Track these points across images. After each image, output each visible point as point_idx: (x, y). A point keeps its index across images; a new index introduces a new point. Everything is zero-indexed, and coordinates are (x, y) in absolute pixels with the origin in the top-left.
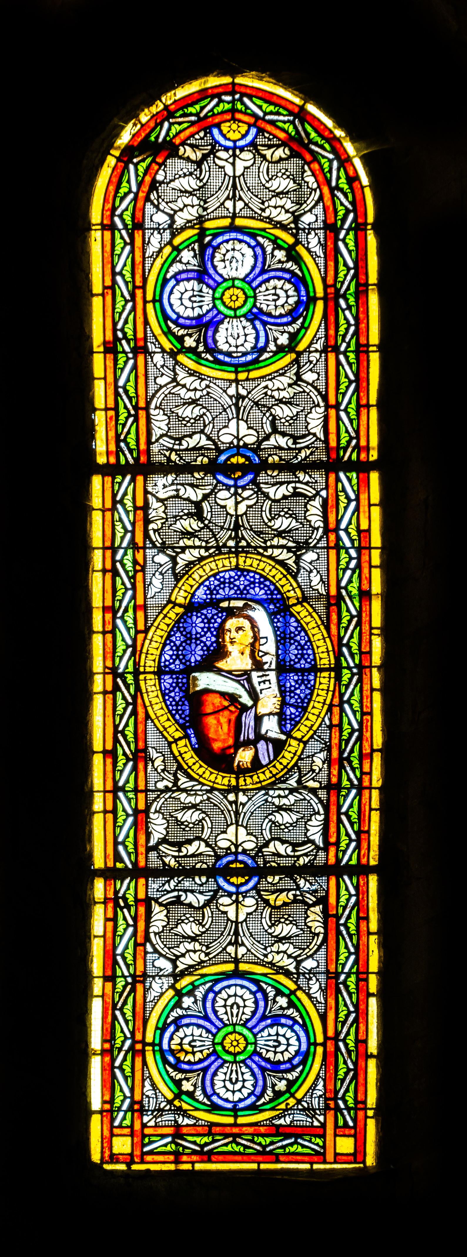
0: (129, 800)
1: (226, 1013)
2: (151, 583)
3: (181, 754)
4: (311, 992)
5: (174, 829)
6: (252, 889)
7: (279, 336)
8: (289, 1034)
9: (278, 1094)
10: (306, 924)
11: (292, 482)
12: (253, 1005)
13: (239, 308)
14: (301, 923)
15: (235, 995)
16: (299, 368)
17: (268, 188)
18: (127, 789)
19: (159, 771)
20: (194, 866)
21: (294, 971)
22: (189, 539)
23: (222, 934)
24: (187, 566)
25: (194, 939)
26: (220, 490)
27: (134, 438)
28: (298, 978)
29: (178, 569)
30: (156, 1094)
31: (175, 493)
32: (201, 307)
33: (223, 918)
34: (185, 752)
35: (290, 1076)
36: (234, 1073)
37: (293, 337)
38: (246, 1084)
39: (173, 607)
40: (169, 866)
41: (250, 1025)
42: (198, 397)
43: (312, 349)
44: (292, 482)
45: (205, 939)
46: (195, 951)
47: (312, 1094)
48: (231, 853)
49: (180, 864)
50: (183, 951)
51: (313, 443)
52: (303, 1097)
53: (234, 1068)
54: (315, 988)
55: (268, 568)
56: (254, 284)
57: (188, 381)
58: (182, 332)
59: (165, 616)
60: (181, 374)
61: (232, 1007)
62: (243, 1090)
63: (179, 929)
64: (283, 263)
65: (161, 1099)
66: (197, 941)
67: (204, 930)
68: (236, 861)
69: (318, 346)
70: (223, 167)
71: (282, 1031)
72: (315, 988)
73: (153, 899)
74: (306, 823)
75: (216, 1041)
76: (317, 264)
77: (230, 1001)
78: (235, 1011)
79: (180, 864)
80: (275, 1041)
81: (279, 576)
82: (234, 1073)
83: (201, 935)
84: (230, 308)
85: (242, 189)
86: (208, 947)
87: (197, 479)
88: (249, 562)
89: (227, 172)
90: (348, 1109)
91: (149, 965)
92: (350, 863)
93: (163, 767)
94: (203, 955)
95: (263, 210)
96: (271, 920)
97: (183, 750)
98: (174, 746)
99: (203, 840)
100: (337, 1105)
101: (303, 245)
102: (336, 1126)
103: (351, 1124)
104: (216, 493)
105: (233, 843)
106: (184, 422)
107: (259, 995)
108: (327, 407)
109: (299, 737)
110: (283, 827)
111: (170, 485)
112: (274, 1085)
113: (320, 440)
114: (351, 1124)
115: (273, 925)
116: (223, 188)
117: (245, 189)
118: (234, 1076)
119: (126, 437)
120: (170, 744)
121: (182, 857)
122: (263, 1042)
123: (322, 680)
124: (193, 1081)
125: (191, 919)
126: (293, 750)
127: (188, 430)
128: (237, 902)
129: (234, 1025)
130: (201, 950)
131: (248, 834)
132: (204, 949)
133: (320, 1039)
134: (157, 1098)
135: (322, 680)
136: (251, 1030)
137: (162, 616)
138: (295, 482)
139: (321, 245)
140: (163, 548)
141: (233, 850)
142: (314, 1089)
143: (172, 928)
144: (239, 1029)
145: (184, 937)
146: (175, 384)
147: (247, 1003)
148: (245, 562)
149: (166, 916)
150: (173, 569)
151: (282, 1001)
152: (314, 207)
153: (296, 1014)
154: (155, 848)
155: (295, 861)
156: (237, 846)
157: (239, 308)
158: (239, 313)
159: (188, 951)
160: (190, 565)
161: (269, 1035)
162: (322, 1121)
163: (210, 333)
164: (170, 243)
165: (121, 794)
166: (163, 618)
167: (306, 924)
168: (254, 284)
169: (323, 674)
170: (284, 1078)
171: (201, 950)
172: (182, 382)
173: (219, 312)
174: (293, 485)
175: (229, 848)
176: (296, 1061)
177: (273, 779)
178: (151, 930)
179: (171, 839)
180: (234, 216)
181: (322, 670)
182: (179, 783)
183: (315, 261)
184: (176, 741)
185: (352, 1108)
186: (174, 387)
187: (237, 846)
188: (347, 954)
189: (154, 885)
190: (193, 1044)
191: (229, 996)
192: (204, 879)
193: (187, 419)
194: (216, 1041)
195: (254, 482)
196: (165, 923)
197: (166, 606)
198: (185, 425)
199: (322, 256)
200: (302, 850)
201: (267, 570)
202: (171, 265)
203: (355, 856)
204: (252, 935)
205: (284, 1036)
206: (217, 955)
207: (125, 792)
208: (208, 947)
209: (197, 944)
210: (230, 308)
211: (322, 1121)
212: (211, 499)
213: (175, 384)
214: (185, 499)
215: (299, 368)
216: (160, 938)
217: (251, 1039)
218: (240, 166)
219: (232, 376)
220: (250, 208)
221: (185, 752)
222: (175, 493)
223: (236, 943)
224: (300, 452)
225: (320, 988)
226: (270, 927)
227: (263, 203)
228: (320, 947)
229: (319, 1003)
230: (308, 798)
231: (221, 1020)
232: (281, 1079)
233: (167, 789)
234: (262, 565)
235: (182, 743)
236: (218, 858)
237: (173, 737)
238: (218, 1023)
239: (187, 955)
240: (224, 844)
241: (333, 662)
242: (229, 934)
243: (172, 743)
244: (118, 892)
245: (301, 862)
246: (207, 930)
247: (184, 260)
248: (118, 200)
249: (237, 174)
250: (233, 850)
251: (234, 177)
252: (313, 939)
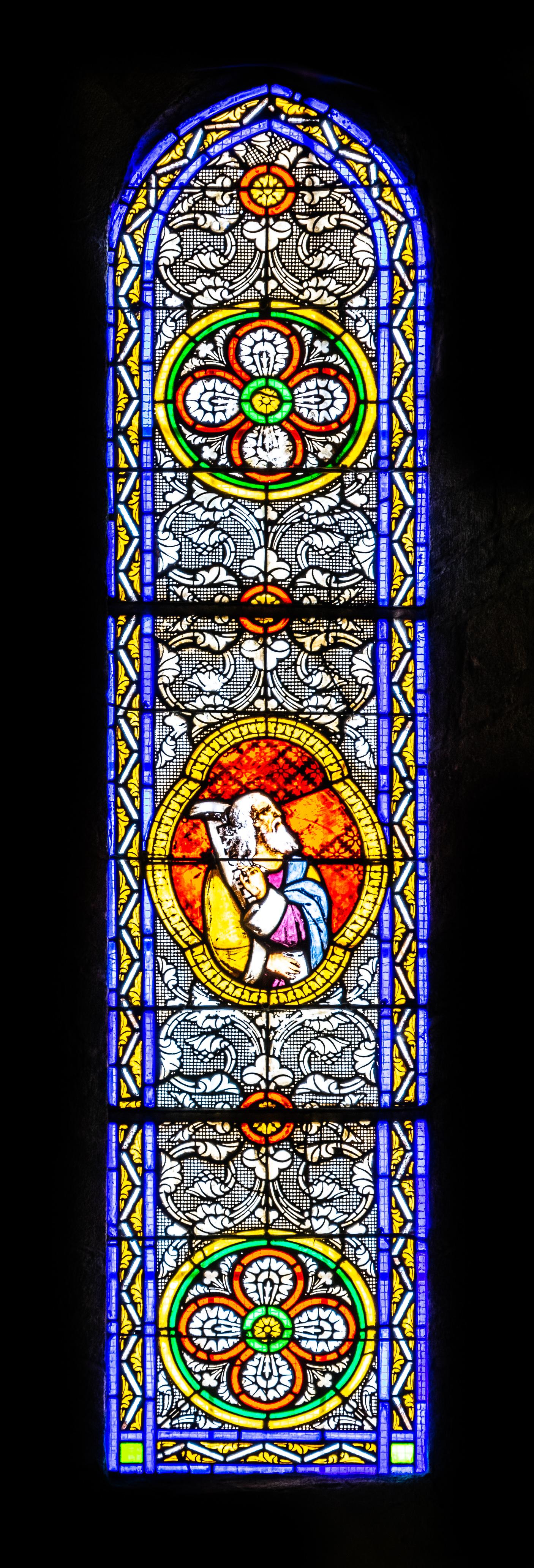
0: (132, 869)
1: (257, 1291)
2: (161, 749)
3: (197, 964)
4: (359, 1263)
5: (188, 1061)
6: (286, 211)
7: (321, 448)
8: (334, 1317)
9: (321, 1392)
10: (350, 674)
11: (336, 212)
12: (287, 351)
13: (272, 413)
14: (345, 673)
15: (269, 1270)
16: (343, 487)
17: (308, 685)
18: (129, 855)
19: (171, 987)
20: (213, 599)
21: (337, 730)
22: (209, 278)
23: (249, 267)
24: (205, 729)
25: (214, 1201)
26: (248, 221)
27: (140, 1217)
28: (342, 740)
29: (195, 732)
30: (172, 1390)
31: (192, 1150)
32: (224, 412)
33: (250, 248)
34: (203, 962)
35: (335, 1369)
36: (268, 1293)
37: (338, 449)
38: (282, 1380)
39: (187, 782)
40: (182, 1104)
41: (286, 1307)
42: (219, 1026)
43: (360, 466)
44: (336, 212)
45: (228, 272)
46: (215, 288)
47: (362, 1391)
48: (261, 1091)
49: (195, 596)
50: (202, 1216)
51: (360, 582)
52: (351, 1395)
53: (267, 1360)
54: (364, 1258)
55: (304, 737)
56: (293, 1313)
57: (206, 498)
58: (199, 440)
59: (177, 793)
60: (198, 490)
61: (264, 1284)
62: (279, 1387)
63: (196, 260)
64: (325, 355)
65: (178, 1395)
66: (218, 275)
67: (227, 1189)
68: (266, 1099)
69: (368, 461)
70: (253, 1169)
71: (209, 418)
72: (364, 1258)
73: (163, 1151)
74: (353, 1052)
75: (243, 397)
76: (368, 1285)
77: (263, 1277)
78: (264, 360)
79: (195, 596)
80: (216, 405)
81: (319, 746)
82: (268, 1293)
83: (222, 268)
84: (260, 413)
85: (275, 266)
86: (231, 283)
87: (219, 625)
88: (281, 729)
89: (258, 1174)
90: (407, 1339)
91: (159, 497)
92: (408, 1099)
93: (175, 983)
94: (225, 293)
95: (301, 292)
96: (308, 249)
97: (200, 959)
98: (188, 953)
99: (226, 1074)
100: (392, 1334)
101: (351, 1262)
102: (391, 1430)
103: (410, 1427)
104: (243, 224)
105: (262, 1078)
106: (201, 1057)
107: (293, 340)
108: (378, 538)
109: (344, 944)
110: (322, 552)
111: (347, 1094)
112: (316, 1381)
113: (369, 579)
114: (410, 1427)
115: (311, 255)
116: (253, 684)
117: (279, 265)
118: (267, 1370)
119: (129, 1357)
120: (183, 951)
121: (197, 587)
122: (302, 1330)
123: (373, 875)
124: (216, 1374)
125: (211, 1177)
126: (199, 767)
127: (205, 561)
128: (266, 574)
129: (267, 1306)
130: (223, 287)
131: (282, 1067)
132: (227, 284)
133: (372, 1321)
134: (173, 1396)
135: (373, 875)
136: (287, 1312)
137: (172, 793)
138: (340, 213)
139: (373, 1261)
140: (176, 710)
141: (262, 579)
142: (365, 1385)
143: (187, 260)
144: (273, 1311)
145: (333, 1036)
146: (189, 501)
147: (283, 1280)
148: (276, 729)
149: (180, 1172)
150: (189, 733)
151: (326, 1278)
152: (365, 1216)
153: (340, 361)
154: (165, 574)
155: (341, 1101)
156: (268, 1083)
157: (272, 413)
158: (271, 420)
159: (207, 1216)
160: (209, 728)
161: (308, 390)
162: (375, 1424)
163: (235, 446)
164: (184, 332)
165: (123, 862)
166: (175, 796)
167: (350, 674)
168: (293, 1313)
169: (374, 868)
170: (328, 1372)
171: (223, 287)
172: (198, 500)
173: (247, 419)
174: (337, 216)
175: (258, 1085)
176: (344, 1350)
177: (313, 996)
178: (162, 1190)
179: (185, 1071)
180: (267, 1226)
181: (371, 863)
182: (194, 496)
183: (366, 1282)
184: (191, 947)
185: (410, 1338)
186: (189, 505)
187: (267, 226)
188: (402, 1362)
189: (165, 623)
190: (214, 401)
191: (262, 1271)
192: (227, 1127)
193: (205, 1053)
194: (243, 397)
195: (288, 628)
196: (177, 254)
197: (178, 781)
198: (202, 1061)
199: (374, 348)
200: (347, 581)
201: (303, 739)
202: (186, 360)
203: (411, 456)
204: (284, 267)
205: (206, 412)
206: (244, 292)
207: (128, 860)
208: (231, 283)
209: (219, 1206)
210: (260, 413)
211: (375, 1424)
212: (237, 1160)
213: (189, 501)
214: (204, 649)
215: (343, 487)
216: (173, 1200)
217: (287, 1323)
218: (274, 1169)
219: (261, 496)
220: (284, 289)
221: (203, 962)
222: (192, 1150)
223: (266, 698)
224: (343, 593)
225: (371, 1258)
226: (307, 257)
227: (301, 283)
228: (369, 1211)
229: (161, 450)
230: (355, 1021)
231: (251, 1300)
232: (324, 1373)
233: (180, 1008)
234: (297, 733)
235: (199, 950)
236: (245, 1096)
237: (187, 943)
238: (248, 1305)
239: (207, 1220)
240: (251, 1080)
241: (384, 852)
242: (257, 267)
243: (186, 949)
244: (119, 639)
245: (347, 1101)
246: (230, 262)
247: (202, 354)
248: (118, 279)
249: (271, 1177)
250: (262, 579)
251: (266, 671)
252: (360, 692)
